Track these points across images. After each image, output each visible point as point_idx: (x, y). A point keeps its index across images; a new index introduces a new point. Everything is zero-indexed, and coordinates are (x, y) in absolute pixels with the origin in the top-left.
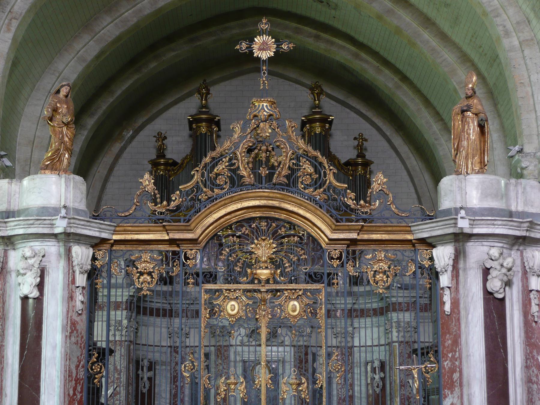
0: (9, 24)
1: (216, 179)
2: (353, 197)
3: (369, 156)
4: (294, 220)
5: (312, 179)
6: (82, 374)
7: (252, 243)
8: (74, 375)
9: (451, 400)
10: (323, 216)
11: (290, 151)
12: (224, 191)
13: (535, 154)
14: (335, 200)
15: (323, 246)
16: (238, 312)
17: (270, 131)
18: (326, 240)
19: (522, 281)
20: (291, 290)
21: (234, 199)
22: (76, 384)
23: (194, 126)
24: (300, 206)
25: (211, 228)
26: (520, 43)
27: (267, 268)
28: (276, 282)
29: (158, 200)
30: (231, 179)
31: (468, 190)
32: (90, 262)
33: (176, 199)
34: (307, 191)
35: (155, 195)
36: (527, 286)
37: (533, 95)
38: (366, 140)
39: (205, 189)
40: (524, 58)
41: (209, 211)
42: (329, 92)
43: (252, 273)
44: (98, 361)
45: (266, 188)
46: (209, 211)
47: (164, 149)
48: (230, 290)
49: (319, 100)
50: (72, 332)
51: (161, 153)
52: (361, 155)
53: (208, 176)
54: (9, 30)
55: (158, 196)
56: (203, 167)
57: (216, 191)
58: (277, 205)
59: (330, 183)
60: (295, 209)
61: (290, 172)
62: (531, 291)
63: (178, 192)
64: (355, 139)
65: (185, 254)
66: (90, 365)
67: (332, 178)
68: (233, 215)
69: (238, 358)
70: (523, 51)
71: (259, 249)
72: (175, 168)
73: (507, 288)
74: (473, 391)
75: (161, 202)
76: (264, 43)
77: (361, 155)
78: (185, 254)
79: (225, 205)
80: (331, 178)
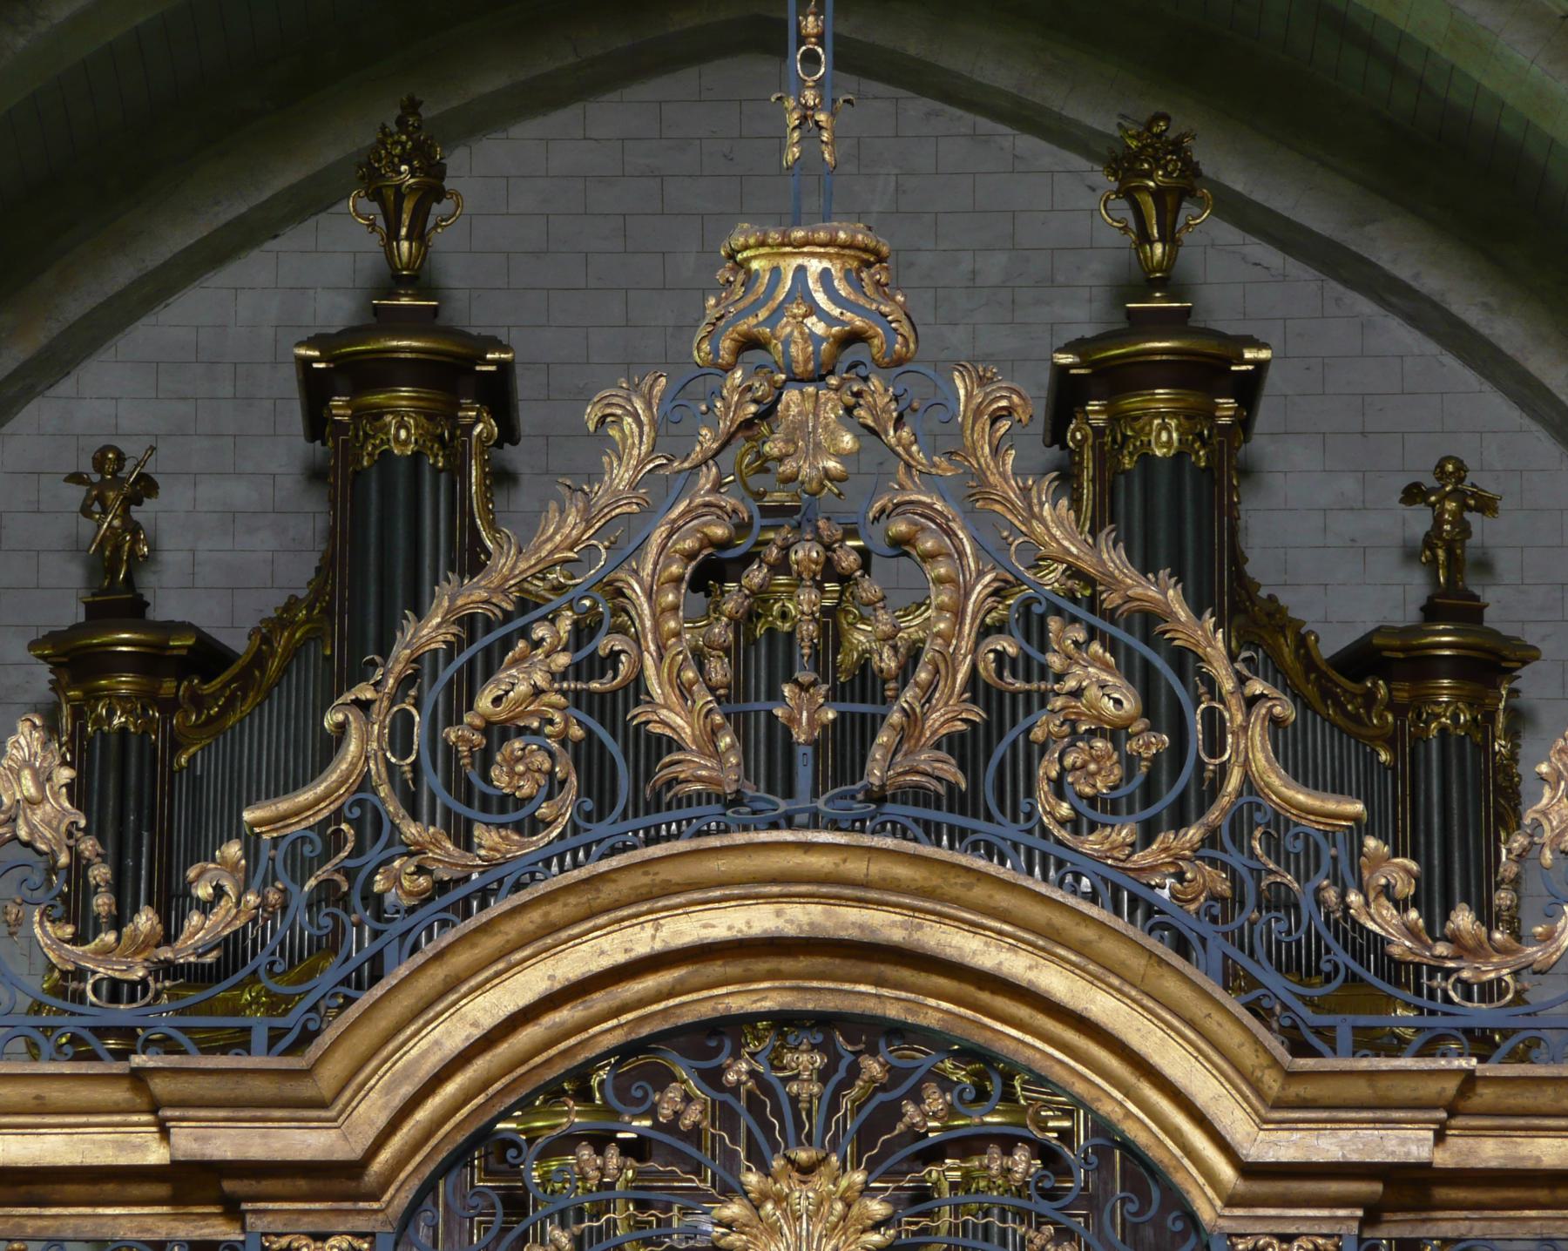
1: (485, 760)
2: (1405, 888)
5: (1130, 762)
7: (729, 1190)
11: (980, 574)
12: (541, 839)
14: (1280, 902)
15: (1207, 1208)
17: (847, 441)
18: (1226, 1172)
21: (608, 893)
23: (339, 406)
25: (450, 1088)
29: (102, 903)
30: (588, 756)
34: (1091, 844)
35: (79, 866)
38: (1486, 505)
39: (411, 830)
42: (1237, 181)
45: (815, 823)
47: (136, 563)
49: (1168, 236)
56: (405, 683)
57: (486, 837)
58: (897, 936)
59: (1248, 781)
60: (1016, 964)
61: (977, 714)
63: (233, 850)
64: (1413, 494)
67: (1261, 760)
68: (600, 1000)
72: (208, 689)
79: (548, 936)
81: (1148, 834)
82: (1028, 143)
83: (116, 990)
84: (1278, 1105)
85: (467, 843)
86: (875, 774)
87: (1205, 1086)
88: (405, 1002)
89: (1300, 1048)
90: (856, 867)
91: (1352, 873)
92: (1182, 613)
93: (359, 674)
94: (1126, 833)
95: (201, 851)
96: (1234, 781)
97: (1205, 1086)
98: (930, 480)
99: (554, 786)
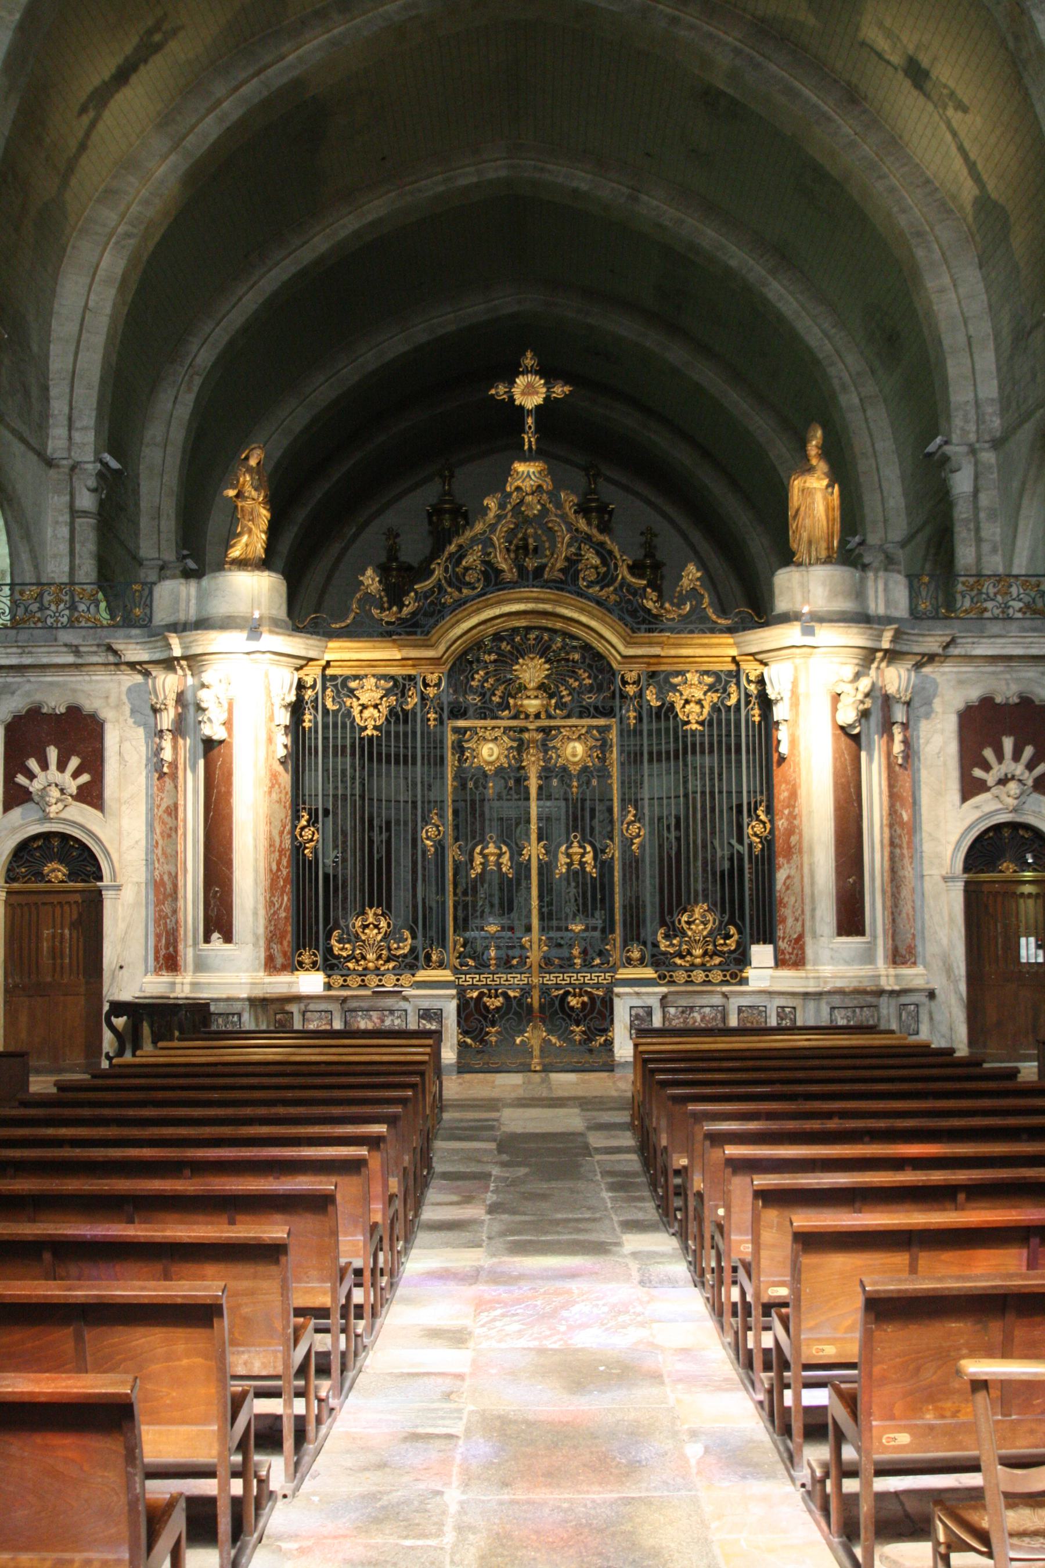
0: (191, 381)
1: (464, 575)
2: (655, 599)
3: (659, 556)
4: (574, 630)
5: (598, 574)
6: (287, 843)
7: (517, 663)
8: (277, 844)
9: (788, 871)
10: (613, 624)
12: (476, 591)
13: (881, 546)
14: (629, 601)
15: (615, 665)
16: (498, 758)
17: (539, 507)
18: (619, 658)
19: (883, 709)
20: (570, 727)
21: (490, 602)
22: (280, 856)
23: (435, 518)
24: (582, 610)
25: (459, 643)
26: (861, 400)
27: (536, 697)
28: (550, 717)
29: (386, 605)
30: (484, 573)
31: (812, 587)
32: (294, 692)
33: (410, 604)
34: (591, 591)
35: (381, 598)
36: (890, 717)
37: (878, 469)
38: (656, 536)
39: (449, 590)
40: (866, 420)
41: (455, 619)
42: (608, 473)
43: (515, 705)
44: (308, 825)
45: (533, 586)
46: (455, 619)
47: (397, 551)
48: (486, 728)
49: (595, 483)
50: (273, 786)
51: (392, 554)
52: (650, 554)
53: (454, 571)
54: (189, 390)
55: (385, 599)
56: (447, 559)
57: (465, 591)
58: (551, 610)
59: (623, 578)
60: (575, 615)
61: (566, 564)
62: (894, 723)
63: (412, 594)
64: (642, 534)
65: (424, 679)
66: (298, 830)
67: (626, 572)
68: (489, 624)
69: (495, 815)
70: (864, 411)
71: (525, 671)
73: (863, 721)
74: (816, 860)
75: (390, 609)
76: (529, 385)
77: (650, 554)
78: (424, 679)
79: (478, 611)
80: (623, 572)
81: (601, 589)
82: (568, 467)
83: (388, 623)
84: (629, 643)
85: (460, 591)
86: (546, 576)
87: (614, 640)
88: (448, 625)
89: (634, 632)
90: (542, 596)
91: (644, 596)
92: (609, 542)
93: (439, 557)
94: (597, 588)
95: (407, 594)
96: (620, 577)
97: (614, 640)
98: (556, 516)
99: (479, 580)
